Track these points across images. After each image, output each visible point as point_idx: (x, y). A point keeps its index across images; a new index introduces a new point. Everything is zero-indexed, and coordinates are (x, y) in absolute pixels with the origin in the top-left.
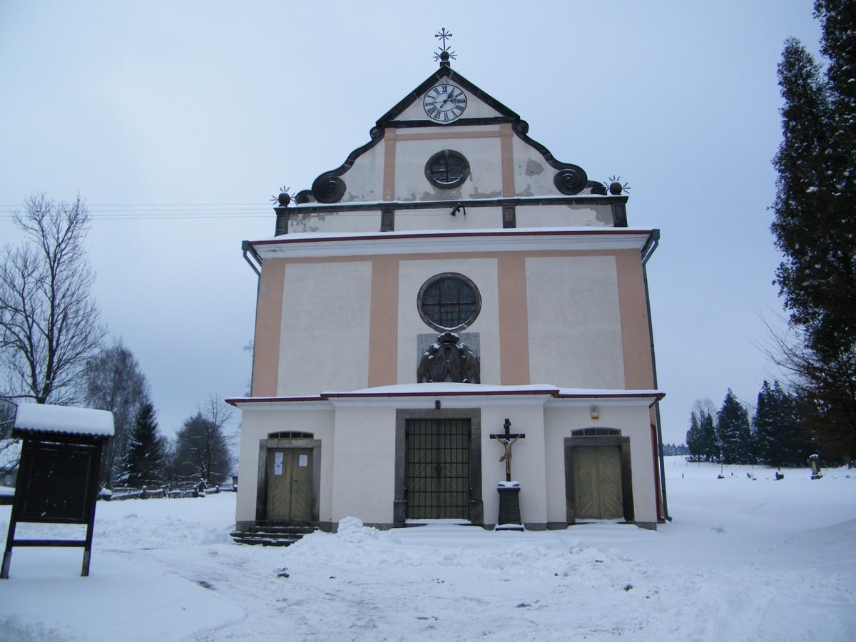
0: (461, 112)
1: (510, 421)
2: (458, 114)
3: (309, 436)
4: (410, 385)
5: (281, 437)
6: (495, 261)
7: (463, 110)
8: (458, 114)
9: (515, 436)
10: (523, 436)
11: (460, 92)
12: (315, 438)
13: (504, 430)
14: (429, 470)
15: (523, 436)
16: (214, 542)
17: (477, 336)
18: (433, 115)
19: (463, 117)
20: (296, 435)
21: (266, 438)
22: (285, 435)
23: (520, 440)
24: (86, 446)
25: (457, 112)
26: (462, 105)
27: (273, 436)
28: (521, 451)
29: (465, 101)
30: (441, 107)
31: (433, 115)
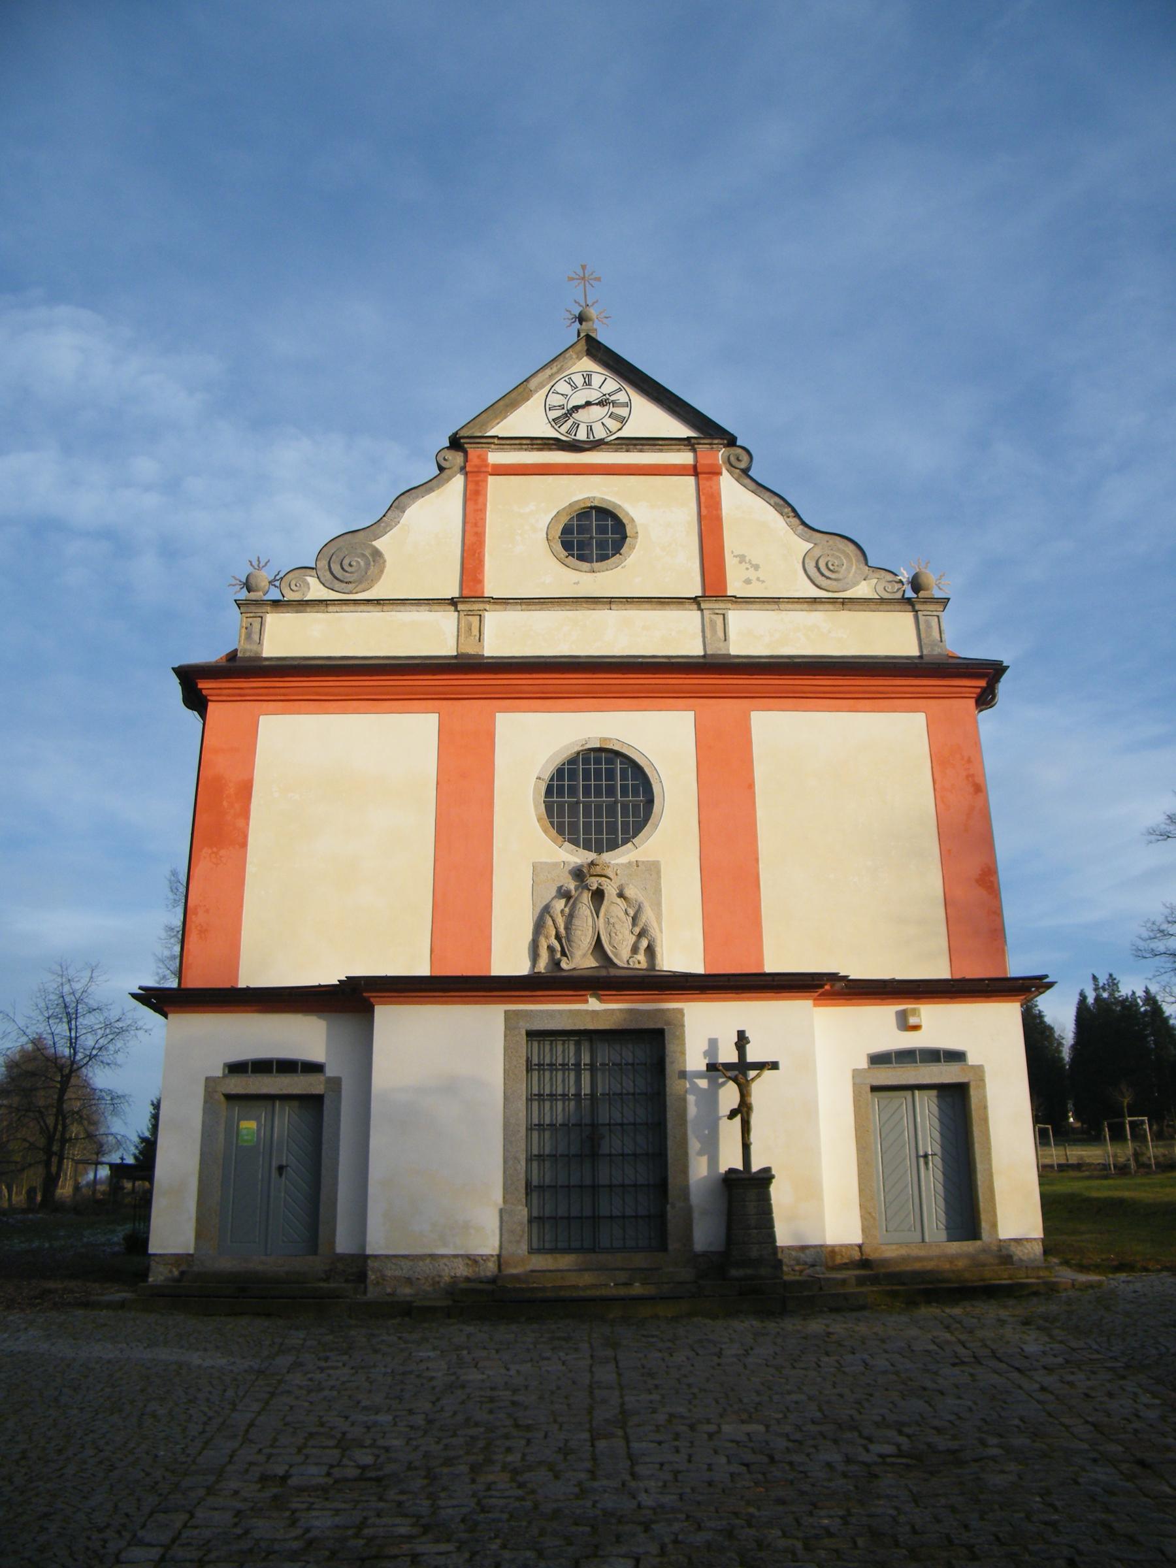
0: (619, 425)
1: (747, 1035)
2: (614, 430)
3: (956, 1056)
4: (207, 1014)
5: (253, 1072)
7: (623, 421)
8: (614, 430)
9: (761, 1066)
10: (774, 1066)
11: (618, 386)
13: (736, 1053)
14: (612, 1144)
15: (774, 1066)
16: (341, 1510)
17: (653, 869)
18: (564, 429)
19: (626, 433)
20: (287, 1067)
21: (220, 1074)
22: (262, 1067)
23: (767, 1073)
24: (641, 789)
25: (613, 425)
26: (623, 412)
27: (236, 1068)
29: (627, 405)
31: (564, 429)
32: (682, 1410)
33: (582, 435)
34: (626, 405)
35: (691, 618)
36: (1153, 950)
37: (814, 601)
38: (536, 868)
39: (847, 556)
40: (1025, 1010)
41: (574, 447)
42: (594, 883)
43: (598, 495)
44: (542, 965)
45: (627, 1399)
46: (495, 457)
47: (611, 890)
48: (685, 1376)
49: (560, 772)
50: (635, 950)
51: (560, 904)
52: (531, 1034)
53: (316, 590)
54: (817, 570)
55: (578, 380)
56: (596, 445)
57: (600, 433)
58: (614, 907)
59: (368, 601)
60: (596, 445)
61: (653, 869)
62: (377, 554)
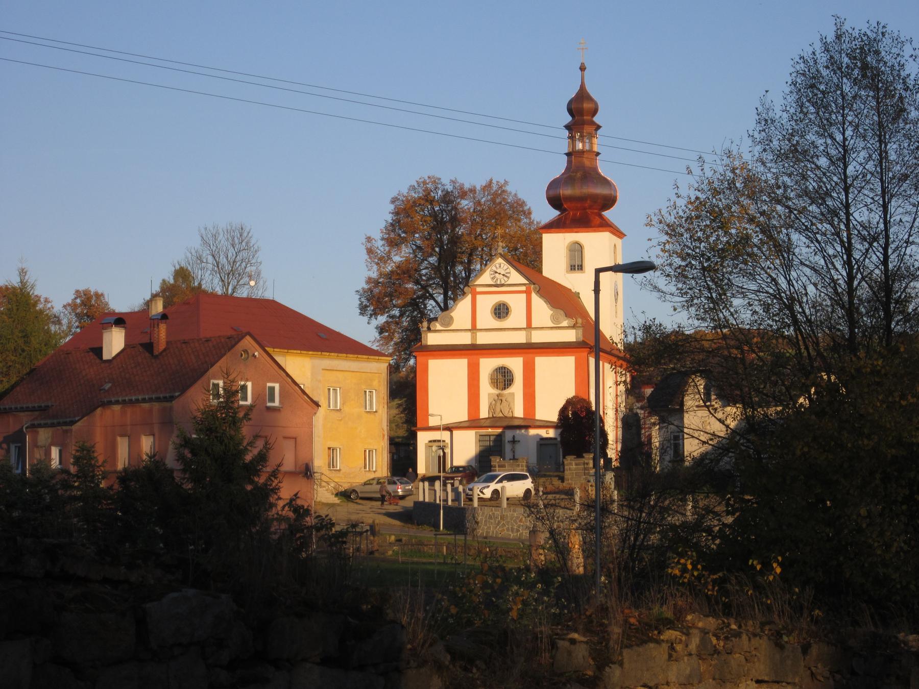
6: (533, 326)
7: (508, 278)
10: (519, 441)
17: (513, 394)
27: (430, 441)
28: (518, 447)
32: (713, 345)
33: (499, 283)
34: (509, 273)
35: (524, 333)
36: (832, 134)
37: (552, 328)
38: (489, 394)
39: (561, 315)
40: (444, 195)
41: (496, 286)
42: (500, 398)
43: (511, 316)
44: (491, 416)
45: (468, 539)
46: (479, 289)
47: (504, 400)
48: (760, 324)
49: (510, 385)
51: (494, 402)
52: (480, 435)
54: (554, 318)
55: (498, 266)
56: (502, 285)
57: (503, 282)
58: (504, 403)
59: (450, 330)
60: (502, 285)
61: (513, 394)
62: (452, 318)
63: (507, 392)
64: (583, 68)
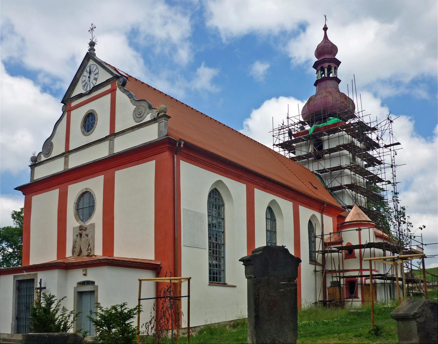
12: (96, 284)
30: (89, 82)
50: (88, 250)
53: (43, 158)
58: (84, 239)
61: (93, 225)
63: (88, 223)
64: (325, 29)
